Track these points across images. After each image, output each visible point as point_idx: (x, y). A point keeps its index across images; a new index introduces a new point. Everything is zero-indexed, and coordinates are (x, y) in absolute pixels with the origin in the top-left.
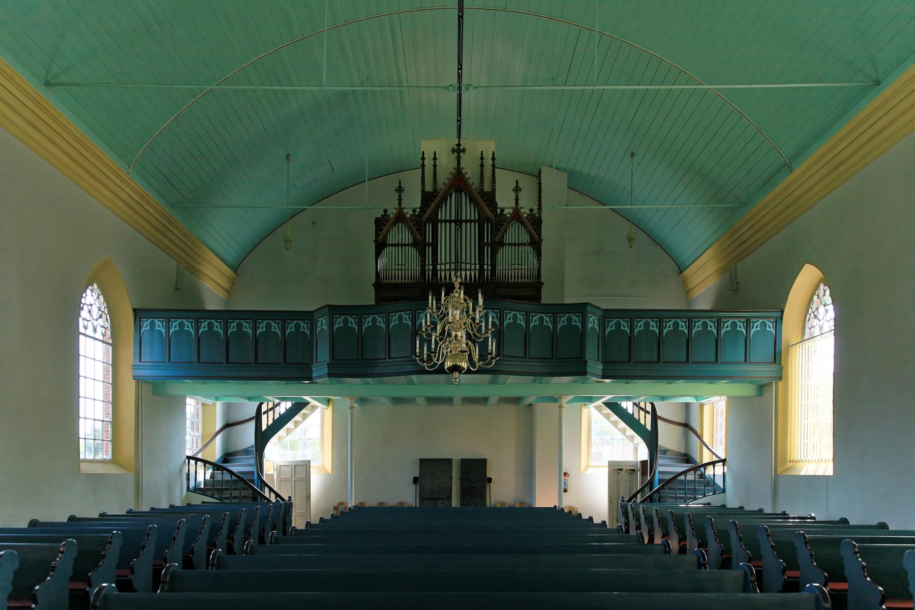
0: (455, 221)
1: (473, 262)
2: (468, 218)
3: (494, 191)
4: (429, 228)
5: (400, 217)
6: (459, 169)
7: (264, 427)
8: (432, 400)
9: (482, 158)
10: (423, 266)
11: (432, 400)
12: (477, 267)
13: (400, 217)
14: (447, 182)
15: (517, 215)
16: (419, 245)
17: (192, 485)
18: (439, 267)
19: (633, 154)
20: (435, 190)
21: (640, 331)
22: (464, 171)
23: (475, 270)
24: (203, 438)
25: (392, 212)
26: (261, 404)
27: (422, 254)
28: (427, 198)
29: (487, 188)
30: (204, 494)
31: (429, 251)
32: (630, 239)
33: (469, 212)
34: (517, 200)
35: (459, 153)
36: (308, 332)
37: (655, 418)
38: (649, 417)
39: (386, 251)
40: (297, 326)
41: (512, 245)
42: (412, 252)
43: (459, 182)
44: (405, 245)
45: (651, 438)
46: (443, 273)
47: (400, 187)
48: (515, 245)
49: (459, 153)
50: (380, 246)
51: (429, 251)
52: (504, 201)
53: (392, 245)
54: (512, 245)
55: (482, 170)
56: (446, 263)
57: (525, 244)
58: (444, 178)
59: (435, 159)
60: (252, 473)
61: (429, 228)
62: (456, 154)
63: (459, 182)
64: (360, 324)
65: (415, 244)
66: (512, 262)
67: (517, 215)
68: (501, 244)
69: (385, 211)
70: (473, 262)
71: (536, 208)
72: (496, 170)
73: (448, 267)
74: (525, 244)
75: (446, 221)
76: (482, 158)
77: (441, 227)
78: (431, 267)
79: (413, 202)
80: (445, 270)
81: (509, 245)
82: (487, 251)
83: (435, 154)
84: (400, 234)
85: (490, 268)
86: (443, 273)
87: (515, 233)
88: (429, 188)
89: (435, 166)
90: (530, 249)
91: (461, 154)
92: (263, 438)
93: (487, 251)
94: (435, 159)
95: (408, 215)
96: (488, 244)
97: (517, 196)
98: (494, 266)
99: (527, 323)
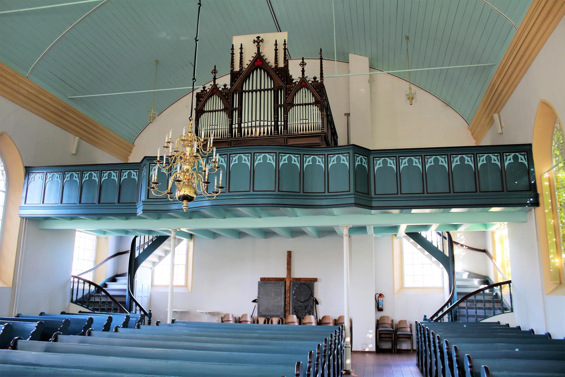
0: (256, 91)
1: (269, 120)
2: (266, 88)
3: (286, 66)
4: (236, 97)
5: (215, 90)
6: (259, 53)
7: (137, 255)
8: (379, 229)
9: (276, 45)
10: (276, 122)
11: (379, 229)
12: (273, 123)
13: (215, 90)
14: (249, 63)
15: (303, 83)
16: (229, 110)
17: (74, 299)
19: (408, 38)
20: (241, 70)
21: (481, 165)
22: (262, 55)
23: (271, 125)
24: (95, 262)
25: (208, 87)
26: (136, 237)
27: (231, 116)
28: (234, 76)
29: (281, 64)
30: (82, 306)
31: (236, 114)
32: (411, 98)
33: (268, 83)
34: (303, 71)
35: (258, 43)
36: (137, 179)
37: (451, 243)
38: (446, 242)
39: (204, 117)
40: (489, 159)
41: (300, 105)
42: (223, 116)
43: (259, 62)
44: (308, 104)
45: (448, 262)
46: (246, 130)
47: (215, 70)
48: (302, 105)
49: (258, 43)
51: (236, 114)
52: (295, 73)
54: (210, 112)
55: (276, 53)
57: (311, 104)
58: (248, 59)
59: (241, 48)
60: (125, 290)
61: (236, 97)
62: (256, 44)
63: (259, 62)
64: (424, 164)
65: (225, 110)
67: (303, 83)
68: (292, 105)
69: (204, 88)
70: (269, 120)
71: (318, 76)
72: (323, 61)
73: (250, 124)
74: (311, 104)
75: (249, 92)
76: (276, 45)
77: (245, 96)
78: (237, 126)
80: (244, 127)
81: (298, 105)
82: (281, 111)
83: (241, 46)
84: (215, 103)
85: (283, 123)
86: (246, 130)
87: (304, 96)
88: (237, 68)
89: (241, 53)
91: (260, 43)
93: (281, 111)
94: (241, 48)
95: (310, 82)
96: (281, 106)
97: (303, 69)
98: (286, 121)
99: (302, 163)
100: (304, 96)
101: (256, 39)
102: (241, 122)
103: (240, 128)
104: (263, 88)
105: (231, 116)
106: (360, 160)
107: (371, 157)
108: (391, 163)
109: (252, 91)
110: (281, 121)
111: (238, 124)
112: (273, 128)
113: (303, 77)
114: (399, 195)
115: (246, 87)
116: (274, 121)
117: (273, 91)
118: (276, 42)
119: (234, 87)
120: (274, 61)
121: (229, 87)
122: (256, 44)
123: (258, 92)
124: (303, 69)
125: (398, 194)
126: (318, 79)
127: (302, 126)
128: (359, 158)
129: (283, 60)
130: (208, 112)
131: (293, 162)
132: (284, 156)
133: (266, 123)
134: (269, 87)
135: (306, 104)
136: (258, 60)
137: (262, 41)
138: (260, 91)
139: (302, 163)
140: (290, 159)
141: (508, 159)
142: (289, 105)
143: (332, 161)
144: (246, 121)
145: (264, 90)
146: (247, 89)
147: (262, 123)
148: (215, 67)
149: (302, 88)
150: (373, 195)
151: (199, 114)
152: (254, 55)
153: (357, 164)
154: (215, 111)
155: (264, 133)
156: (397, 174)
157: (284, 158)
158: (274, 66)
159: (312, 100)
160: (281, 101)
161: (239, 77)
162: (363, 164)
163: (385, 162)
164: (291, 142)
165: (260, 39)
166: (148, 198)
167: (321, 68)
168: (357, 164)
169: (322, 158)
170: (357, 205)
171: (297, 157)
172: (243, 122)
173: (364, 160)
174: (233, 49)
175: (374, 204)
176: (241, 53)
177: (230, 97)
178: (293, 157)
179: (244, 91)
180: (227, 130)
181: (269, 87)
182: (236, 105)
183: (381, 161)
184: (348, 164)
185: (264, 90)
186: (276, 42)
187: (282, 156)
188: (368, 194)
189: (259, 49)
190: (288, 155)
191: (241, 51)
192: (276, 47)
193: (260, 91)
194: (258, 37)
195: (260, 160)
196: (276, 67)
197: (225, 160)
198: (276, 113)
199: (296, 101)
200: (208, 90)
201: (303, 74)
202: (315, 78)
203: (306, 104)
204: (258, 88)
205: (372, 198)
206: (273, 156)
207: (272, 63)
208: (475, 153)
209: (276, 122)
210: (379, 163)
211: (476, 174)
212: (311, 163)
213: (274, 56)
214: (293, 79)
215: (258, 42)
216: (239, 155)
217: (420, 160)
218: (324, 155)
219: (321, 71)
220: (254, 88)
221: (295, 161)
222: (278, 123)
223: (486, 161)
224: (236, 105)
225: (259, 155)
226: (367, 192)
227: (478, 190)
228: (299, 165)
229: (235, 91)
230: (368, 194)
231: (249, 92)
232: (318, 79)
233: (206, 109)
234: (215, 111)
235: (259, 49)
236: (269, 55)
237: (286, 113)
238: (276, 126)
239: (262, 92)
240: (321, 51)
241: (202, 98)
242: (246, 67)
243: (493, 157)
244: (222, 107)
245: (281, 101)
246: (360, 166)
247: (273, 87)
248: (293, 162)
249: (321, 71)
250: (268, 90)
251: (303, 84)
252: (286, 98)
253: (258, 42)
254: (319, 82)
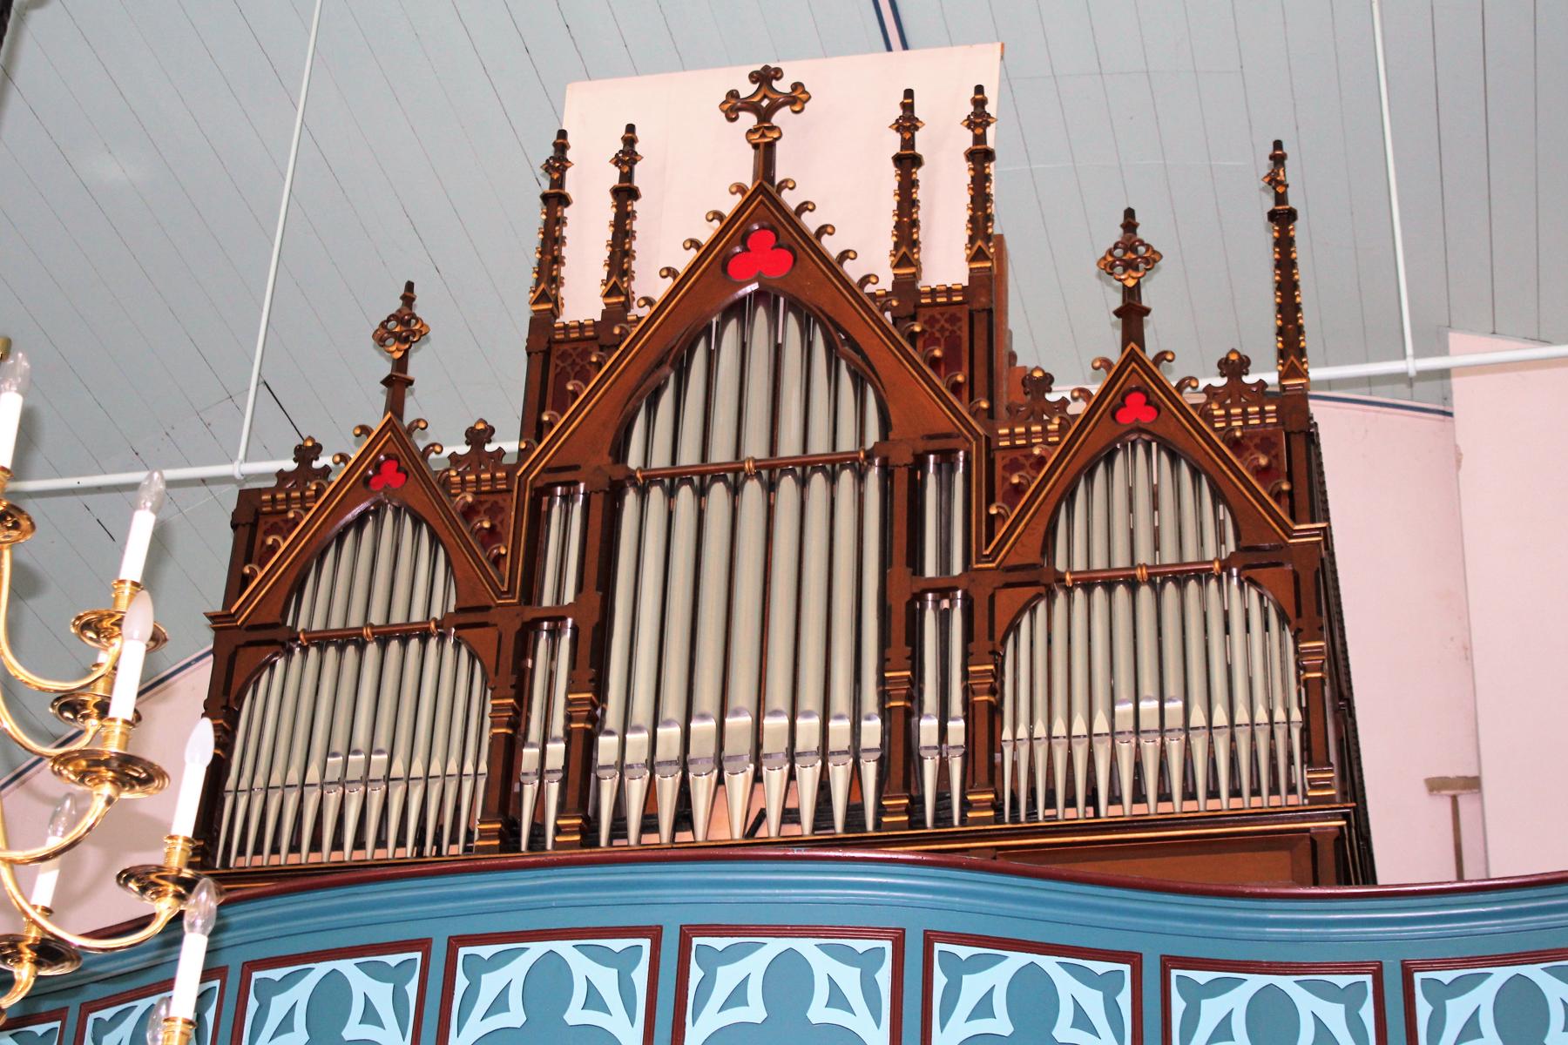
4: (565, 535)
5: (393, 456)
6: (765, 191)
9: (907, 124)
10: (507, 752)
14: (683, 260)
15: (1137, 398)
16: (497, 631)
22: (791, 199)
25: (339, 447)
27: (511, 681)
28: (555, 355)
29: (946, 264)
31: (553, 664)
33: (834, 416)
35: (764, 116)
39: (282, 688)
42: (447, 679)
43: (765, 241)
44: (1181, 578)
49: (764, 116)
50: (248, 644)
51: (553, 664)
53: (322, 641)
57: (1201, 575)
59: (627, 158)
61: (565, 535)
62: (748, 120)
63: (765, 241)
65: (466, 621)
66: (1128, 690)
67: (1137, 398)
68: (1039, 581)
74: (1201, 575)
75: (673, 480)
76: (907, 124)
77: (643, 524)
79: (474, 393)
82: (942, 636)
84: (394, 571)
87: (1142, 509)
89: (625, 194)
90: (1243, 602)
93: (942, 636)
94: (627, 158)
97: (1132, 294)
98: (986, 720)
100: (1142, 509)
101: (747, 89)
102: (596, 724)
105: (511, 681)
109: (702, 479)
111: (568, 735)
113: (1131, 358)
115: (649, 447)
116: (885, 713)
117: (873, 475)
118: (908, 107)
119: (548, 450)
120: (889, 242)
121: (508, 443)
122: (748, 120)
124: (1132, 294)
127: (333, 799)
129: (964, 235)
130: (322, 641)
135: (1158, 579)
137: (797, 98)
138: (771, 472)
142: (1017, 582)
145: (803, 469)
148: (408, 297)
151: (246, 659)
154: (383, 638)
158: (885, 283)
160: (943, 547)
165: (782, 86)
171: (1108, 986)
176: (625, 194)
177: (513, 518)
178: (1067, 986)
180: (473, 795)
181: (847, 443)
182: (561, 582)
185: (803, 469)
186: (908, 107)
187: (957, 971)
189: (766, 154)
193: (771, 472)
194: (765, 77)
195: (738, 996)
196: (905, 286)
197: (399, 998)
198: (900, 649)
199: (1072, 555)
200: (1078, 408)
201: (395, 406)
203: (1158, 579)
206: (866, 965)
207: (871, 259)
209: (507, 752)
213: (892, 203)
214: (1050, 391)
215: (764, 103)
216: (537, 949)
220: (721, 453)
224: (561, 582)
225: (730, 956)
229: (561, 474)
231: (673, 480)
233: (311, 615)
234: (383, 638)
235: (766, 154)
236: (842, 195)
237: (988, 640)
238: (900, 759)
239: (787, 486)
240: (1278, 159)
242: (659, 288)
245: (943, 547)
247: (873, 436)
250: (831, 467)
251: (1136, 412)
252: (982, 530)
253: (764, 103)
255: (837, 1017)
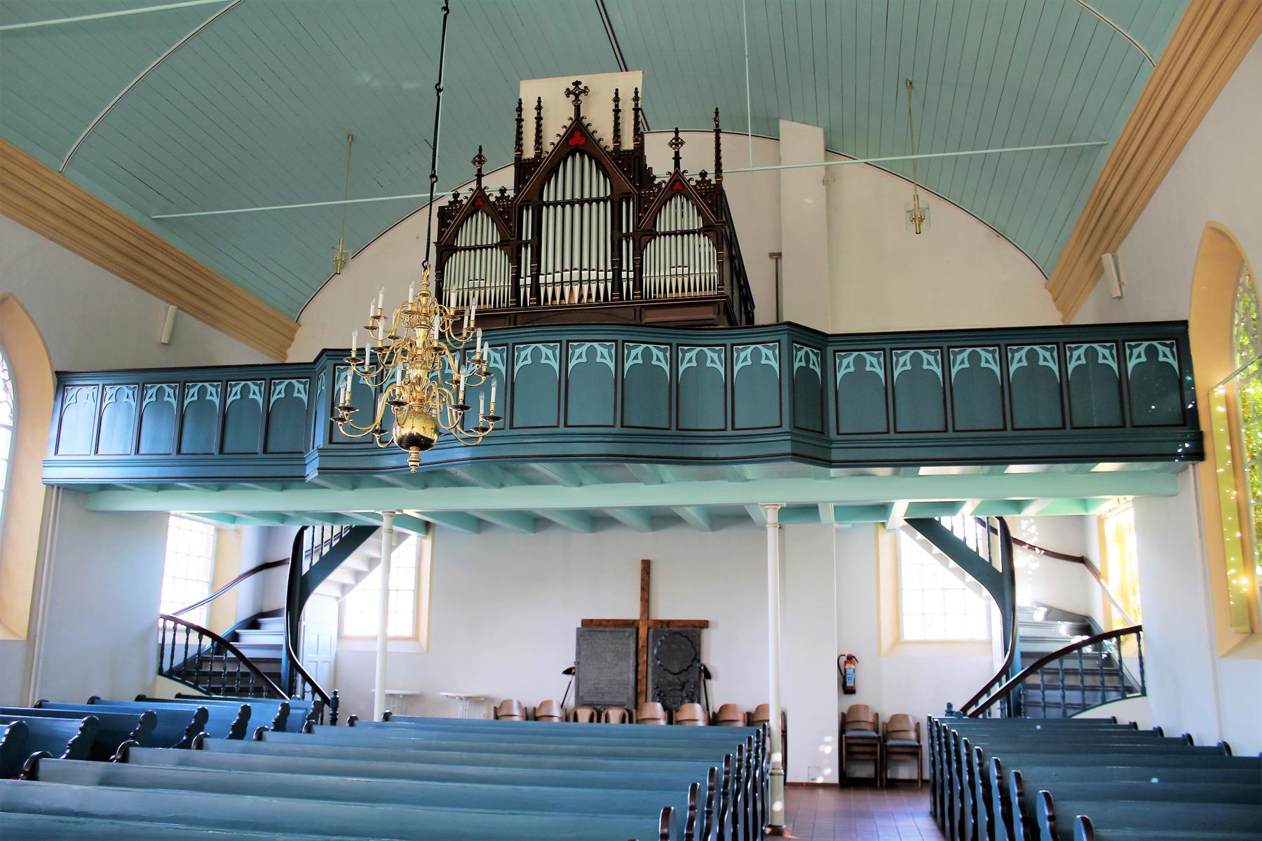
0: (572, 203)
1: (602, 267)
2: (594, 196)
3: (640, 148)
4: (528, 217)
5: (479, 201)
6: (578, 118)
7: (306, 568)
8: (847, 511)
9: (617, 99)
10: (617, 271)
11: (847, 511)
12: (610, 275)
14: (556, 140)
15: (678, 184)
16: (511, 245)
17: (166, 667)
18: (522, 282)
19: (910, 84)
20: (538, 156)
21: (1075, 369)
22: (585, 122)
23: (606, 280)
24: (213, 584)
25: (465, 193)
26: (304, 528)
27: (515, 260)
28: (523, 169)
29: (628, 144)
31: (526, 254)
33: (598, 186)
34: (677, 158)
35: (577, 96)
36: (305, 398)
37: (1008, 543)
38: (997, 540)
39: (455, 261)
40: (1092, 354)
41: (670, 234)
42: (499, 259)
43: (578, 139)
44: (688, 233)
45: (1001, 584)
46: (550, 290)
47: (480, 156)
48: (676, 234)
49: (577, 96)
51: (526, 254)
52: (659, 162)
54: (470, 249)
55: (617, 118)
56: (581, 282)
57: (694, 232)
58: (554, 132)
59: (539, 108)
60: (279, 647)
61: (528, 217)
62: (572, 97)
63: (578, 139)
64: (946, 366)
65: (502, 245)
67: (678, 184)
68: (652, 234)
69: (456, 196)
70: (602, 267)
71: (711, 170)
73: (558, 276)
74: (694, 232)
75: (555, 204)
76: (617, 99)
77: (548, 214)
78: (529, 280)
80: (546, 284)
81: (665, 234)
82: (627, 248)
83: (539, 102)
84: (481, 229)
85: (631, 275)
86: (550, 290)
87: (679, 215)
88: (529, 152)
89: (539, 119)
91: (582, 97)
92: (299, 590)
93: (627, 248)
94: (539, 108)
95: (693, 183)
96: (627, 237)
97: (677, 153)
98: (639, 271)
99: (674, 364)
103: (536, 286)
104: (586, 196)
105: (515, 260)
106: (804, 356)
107: (830, 350)
108: (874, 363)
110: (628, 271)
112: (609, 285)
113: (676, 172)
114: (892, 435)
115: (549, 194)
117: (609, 204)
118: (617, 94)
122: (572, 97)
123: (577, 206)
124: (677, 153)
125: (888, 432)
126: (711, 177)
127: (674, 280)
128: (801, 354)
130: (465, 249)
131: (654, 362)
132: (634, 347)
133: (594, 274)
134: (602, 195)
136: (577, 134)
137: (586, 91)
138: (582, 202)
139: (674, 364)
140: (647, 355)
141: (1135, 354)
142: (646, 234)
143: (741, 358)
144: (550, 270)
145: (590, 201)
146: (552, 199)
147: (585, 273)
149: (674, 195)
150: (833, 435)
151: (445, 255)
152: (568, 123)
153: (797, 365)
154: (481, 249)
155: (590, 296)
156: (886, 388)
157: (633, 353)
159: (697, 223)
160: (628, 225)
161: (534, 173)
162: (811, 366)
163: (860, 362)
164: (650, 317)
165: (581, 87)
166: (331, 442)
167: (718, 151)
168: (797, 365)
169: (719, 352)
170: (796, 456)
172: (543, 271)
173: (812, 357)
174: (520, 109)
175: (836, 455)
176: (539, 119)
178: (655, 351)
179: (544, 204)
180: (508, 290)
182: (527, 234)
183: (851, 358)
184: (776, 367)
185: (590, 201)
186: (617, 94)
188: (822, 433)
190: (644, 346)
191: (539, 114)
192: (617, 106)
198: (617, 253)
199: (661, 226)
200: (465, 202)
201: (677, 165)
202: (703, 174)
204: (577, 196)
205: (831, 442)
206: (609, 348)
207: (608, 141)
208: (1061, 341)
209: (617, 271)
210: (846, 364)
211: (1063, 388)
212: (694, 364)
215: (577, 93)
217: (939, 358)
218: (725, 345)
219: (718, 157)
220: (568, 197)
221: (658, 359)
222: (620, 275)
223: (1086, 358)
224: (527, 234)
226: (819, 429)
227: (1068, 425)
228: (667, 369)
230: (822, 433)
232: (711, 177)
237: (639, 251)
238: (617, 282)
241: (451, 219)
243: (1100, 350)
244: (496, 239)
245: (628, 225)
246: (805, 371)
247: (609, 193)
248: (654, 362)
249: (718, 157)
250: (598, 201)
251: (677, 187)
253: (577, 93)
254: (713, 182)
255: (767, 362)
